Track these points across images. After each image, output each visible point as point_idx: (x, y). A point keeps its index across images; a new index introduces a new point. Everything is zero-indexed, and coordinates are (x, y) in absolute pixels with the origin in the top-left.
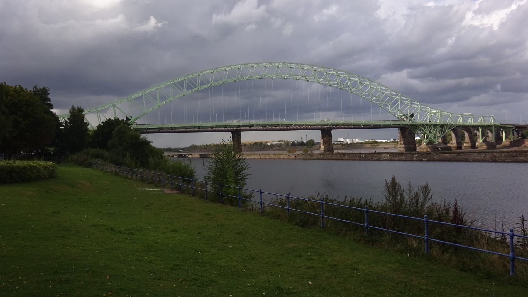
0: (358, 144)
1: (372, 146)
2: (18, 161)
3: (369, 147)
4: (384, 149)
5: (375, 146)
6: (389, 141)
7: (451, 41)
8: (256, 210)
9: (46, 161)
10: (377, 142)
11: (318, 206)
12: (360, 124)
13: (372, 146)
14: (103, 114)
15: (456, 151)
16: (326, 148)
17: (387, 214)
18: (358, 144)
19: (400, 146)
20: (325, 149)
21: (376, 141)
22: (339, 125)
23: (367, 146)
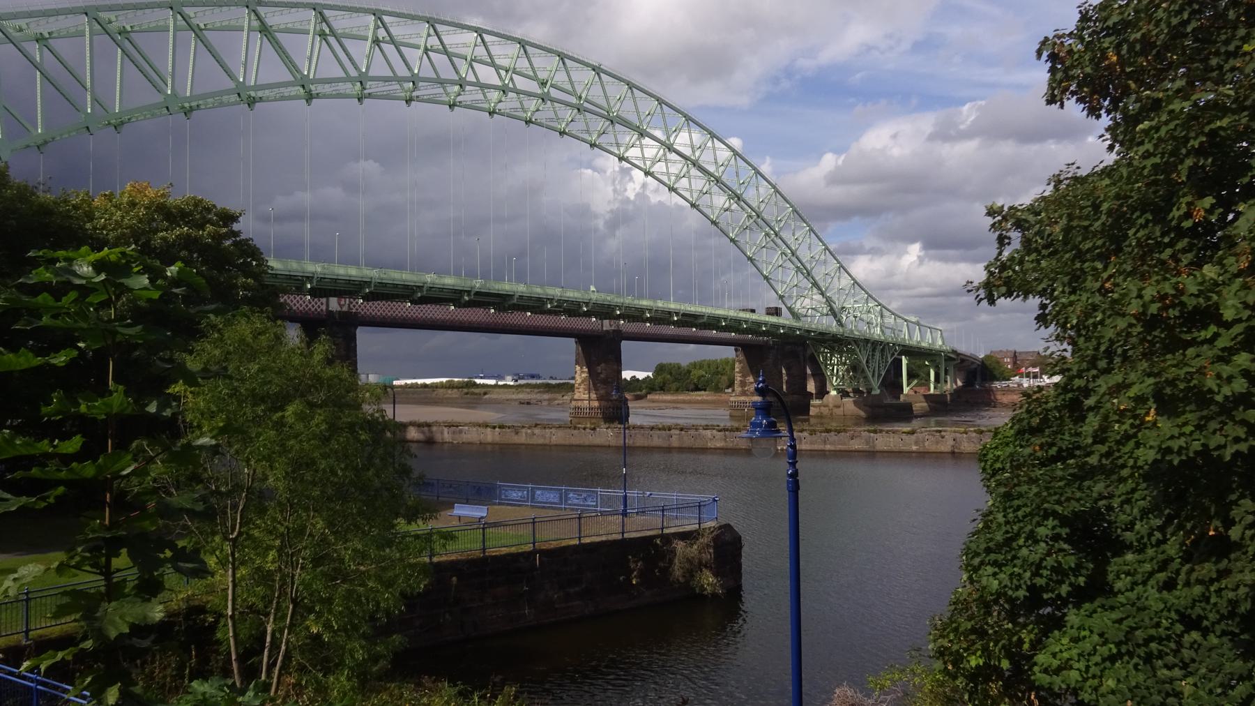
0: (417, 387)
1: (467, 394)
2: (80, 444)
3: (454, 396)
4: (521, 403)
5: (473, 394)
6: (501, 383)
7: (1209, 98)
8: (697, 572)
9: (455, 442)
10: (475, 385)
11: (348, 608)
12: (670, 313)
13: (467, 394)
14: (392, 75)
15: (672, 418)
16: (608, 400)
17: (236, 635)
18: (417, 387)
19: (742, 398)
20: (604, 403)
21: (475, 382)
22: (304, 284)
23: (447, 393)
